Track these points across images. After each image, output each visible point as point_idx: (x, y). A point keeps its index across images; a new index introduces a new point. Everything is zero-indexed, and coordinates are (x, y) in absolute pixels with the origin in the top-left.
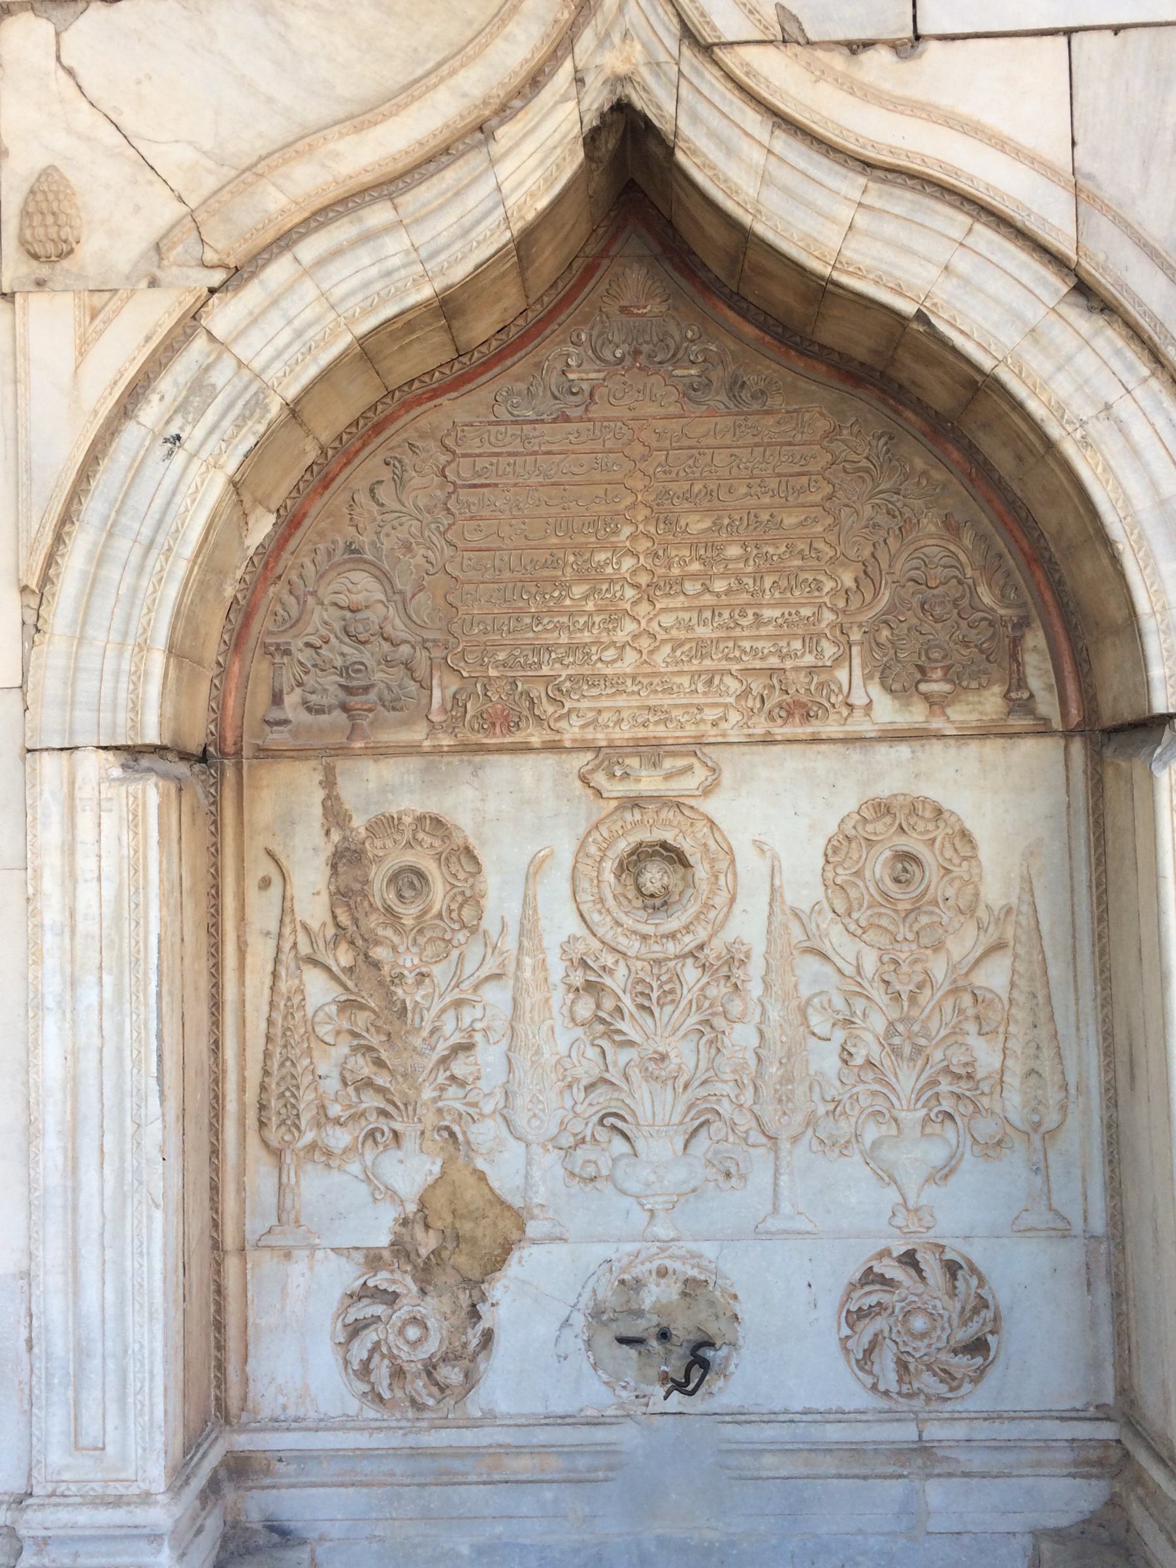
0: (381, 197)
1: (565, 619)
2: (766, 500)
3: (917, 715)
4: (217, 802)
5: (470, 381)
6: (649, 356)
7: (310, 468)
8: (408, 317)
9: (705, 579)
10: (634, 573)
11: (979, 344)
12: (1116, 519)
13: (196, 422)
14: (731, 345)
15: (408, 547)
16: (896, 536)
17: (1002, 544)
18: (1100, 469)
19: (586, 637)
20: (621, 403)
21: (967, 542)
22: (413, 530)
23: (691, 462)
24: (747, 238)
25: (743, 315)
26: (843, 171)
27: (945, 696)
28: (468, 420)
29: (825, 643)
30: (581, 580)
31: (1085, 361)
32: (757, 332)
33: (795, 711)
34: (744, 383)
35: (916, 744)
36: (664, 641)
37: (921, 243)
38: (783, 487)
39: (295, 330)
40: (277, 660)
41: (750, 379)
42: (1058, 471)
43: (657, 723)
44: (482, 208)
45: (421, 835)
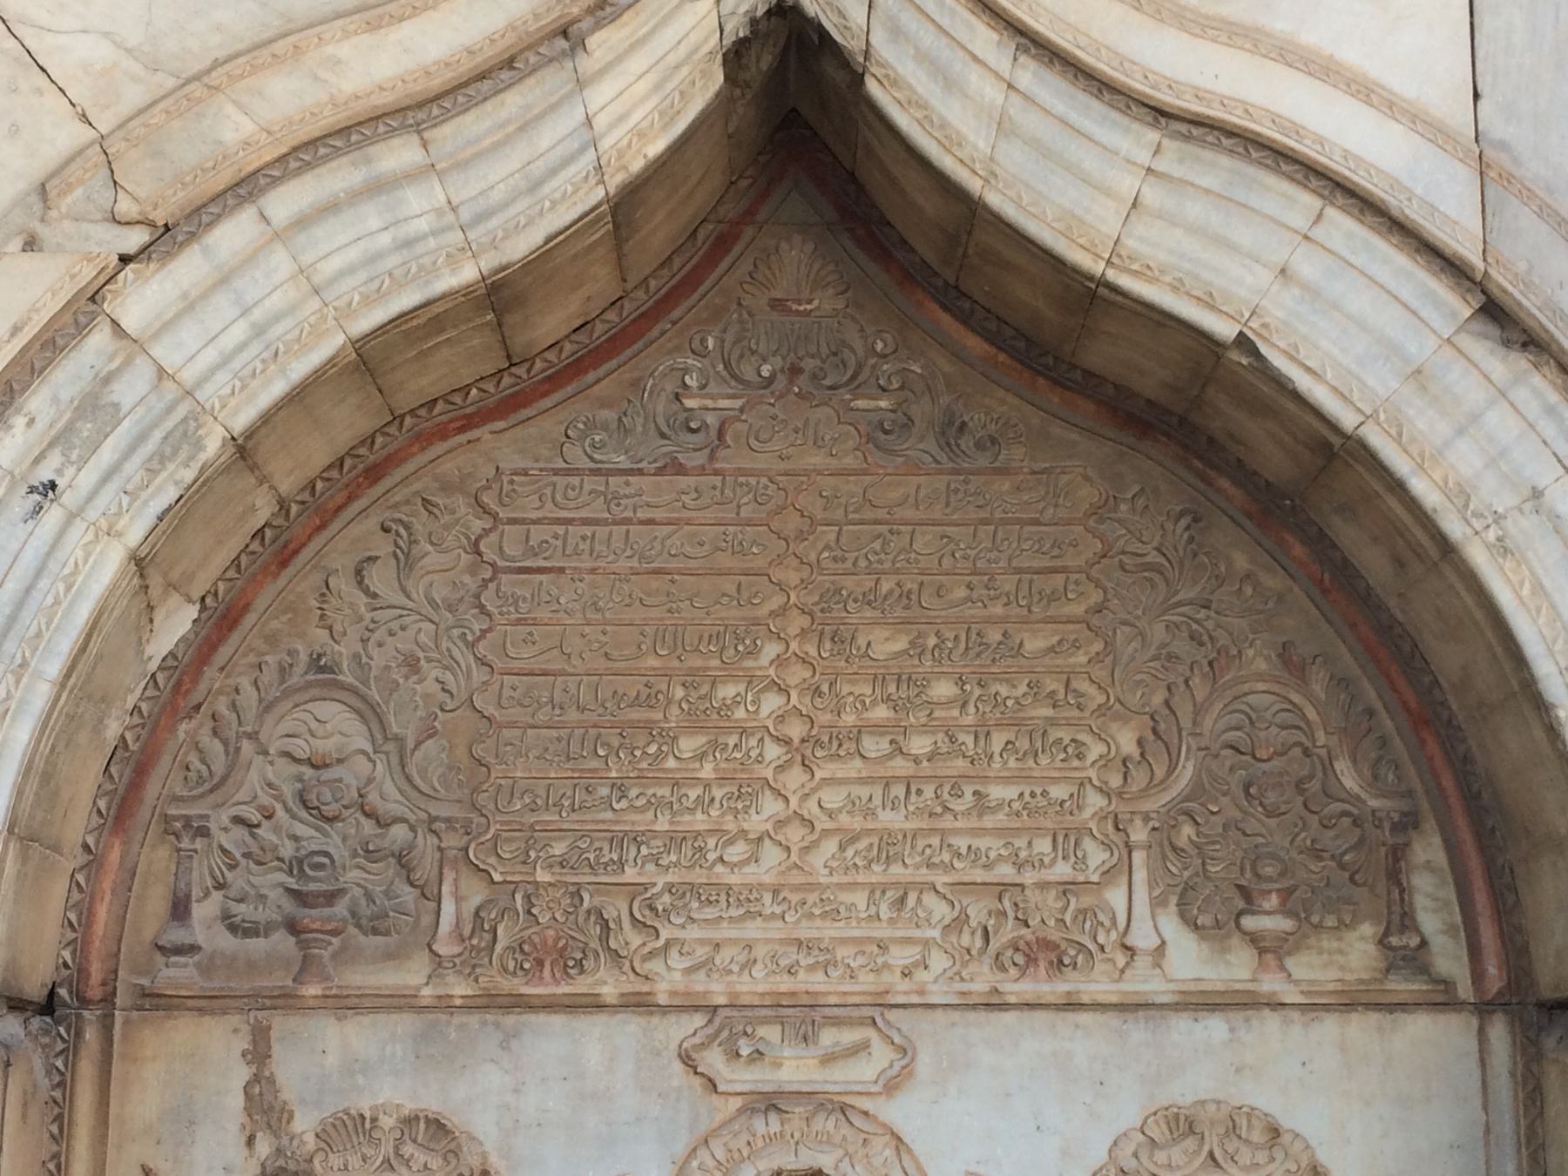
0: (404, 128)
1: (664, 791)
2: (998, 610)
3: (1236, 968)
4: (64, 1083)
5: (524, 405)
6: (814, 377)
7: (260, 532)
8: (437, 309)
9: (897, 733)
10: (781, 719)
11: (1335, 389)
12: (1553, 669)
13: (83, 462)
14: (944, 364)
15: (412, 665)
16: (1204, 676)
17: (1373, 694)
18: (1526, 592)
19: (699, 821)
20: (768, 447)
21: (1318, 688)
22: (423, 638)
23: (877, 545)
24: (973, 213)
25: (965, 319)
26: (1125, 121)
27: (1284, 937)
28: (521, 464)
29: (1088, 845)
30: (695, 729)
31: (1502, 423)
32: (986, 346)
33: (1042, 954)
34: (964, 424)
35: (1238, 1017)
36: (826, 833)
37: (1245, 234)
38: (1024, 591)
39: (253, 325)
40: (185, 843)
41: (975, 418)
42: (1464, 593)
43: (811, 968)
44: (560, 151)
45: (408, 1149)
